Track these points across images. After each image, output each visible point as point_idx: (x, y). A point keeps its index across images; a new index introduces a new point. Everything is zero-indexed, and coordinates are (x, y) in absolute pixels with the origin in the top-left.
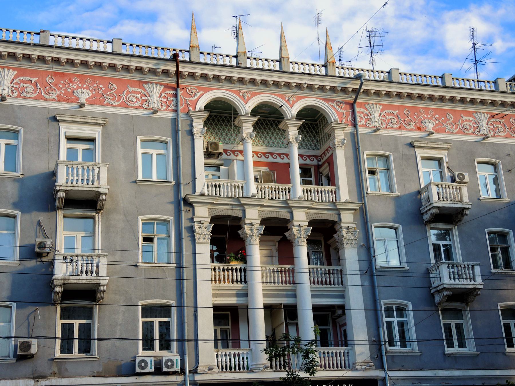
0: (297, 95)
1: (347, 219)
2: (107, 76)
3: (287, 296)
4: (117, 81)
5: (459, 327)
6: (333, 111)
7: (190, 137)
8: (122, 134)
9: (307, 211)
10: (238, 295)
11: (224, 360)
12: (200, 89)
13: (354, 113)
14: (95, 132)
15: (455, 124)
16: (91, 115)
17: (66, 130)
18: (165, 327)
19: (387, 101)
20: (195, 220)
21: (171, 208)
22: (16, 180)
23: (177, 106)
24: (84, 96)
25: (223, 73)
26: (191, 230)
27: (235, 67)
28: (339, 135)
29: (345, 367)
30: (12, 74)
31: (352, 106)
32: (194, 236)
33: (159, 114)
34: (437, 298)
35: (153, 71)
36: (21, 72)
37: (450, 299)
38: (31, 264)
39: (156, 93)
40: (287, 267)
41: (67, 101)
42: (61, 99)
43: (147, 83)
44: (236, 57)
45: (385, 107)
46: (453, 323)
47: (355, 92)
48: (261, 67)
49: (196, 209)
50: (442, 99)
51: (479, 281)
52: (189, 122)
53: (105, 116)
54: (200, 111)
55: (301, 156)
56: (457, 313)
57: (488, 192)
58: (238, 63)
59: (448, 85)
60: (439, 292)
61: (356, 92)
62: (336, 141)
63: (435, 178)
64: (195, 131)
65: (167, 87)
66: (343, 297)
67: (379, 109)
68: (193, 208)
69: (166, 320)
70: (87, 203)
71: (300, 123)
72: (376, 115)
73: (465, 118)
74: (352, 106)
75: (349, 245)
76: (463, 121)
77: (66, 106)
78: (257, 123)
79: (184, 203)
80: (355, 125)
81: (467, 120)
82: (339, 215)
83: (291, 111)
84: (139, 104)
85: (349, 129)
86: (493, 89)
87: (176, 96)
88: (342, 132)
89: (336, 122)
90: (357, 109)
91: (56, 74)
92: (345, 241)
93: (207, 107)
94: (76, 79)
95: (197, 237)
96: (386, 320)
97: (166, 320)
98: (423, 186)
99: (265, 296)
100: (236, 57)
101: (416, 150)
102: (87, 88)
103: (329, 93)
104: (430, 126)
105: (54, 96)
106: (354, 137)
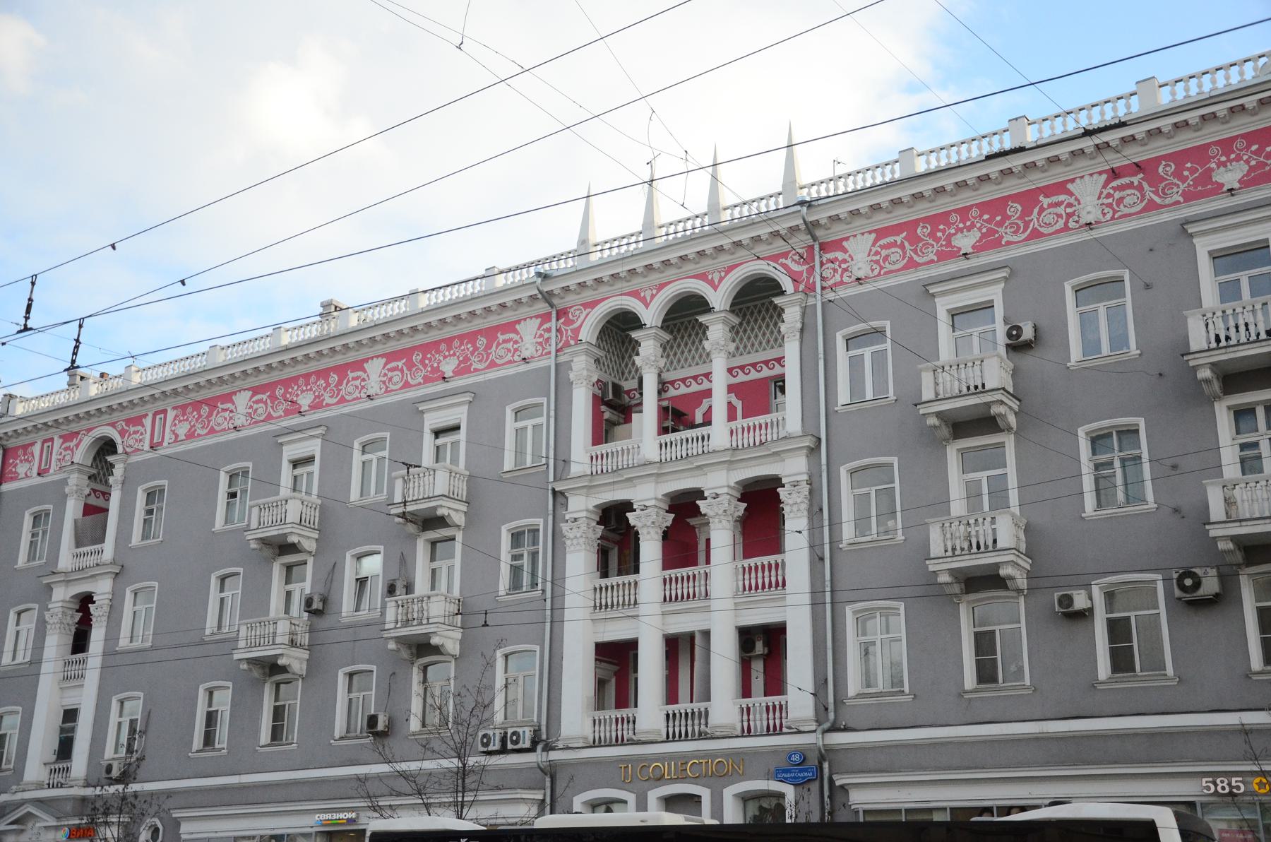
92: (568, 542)
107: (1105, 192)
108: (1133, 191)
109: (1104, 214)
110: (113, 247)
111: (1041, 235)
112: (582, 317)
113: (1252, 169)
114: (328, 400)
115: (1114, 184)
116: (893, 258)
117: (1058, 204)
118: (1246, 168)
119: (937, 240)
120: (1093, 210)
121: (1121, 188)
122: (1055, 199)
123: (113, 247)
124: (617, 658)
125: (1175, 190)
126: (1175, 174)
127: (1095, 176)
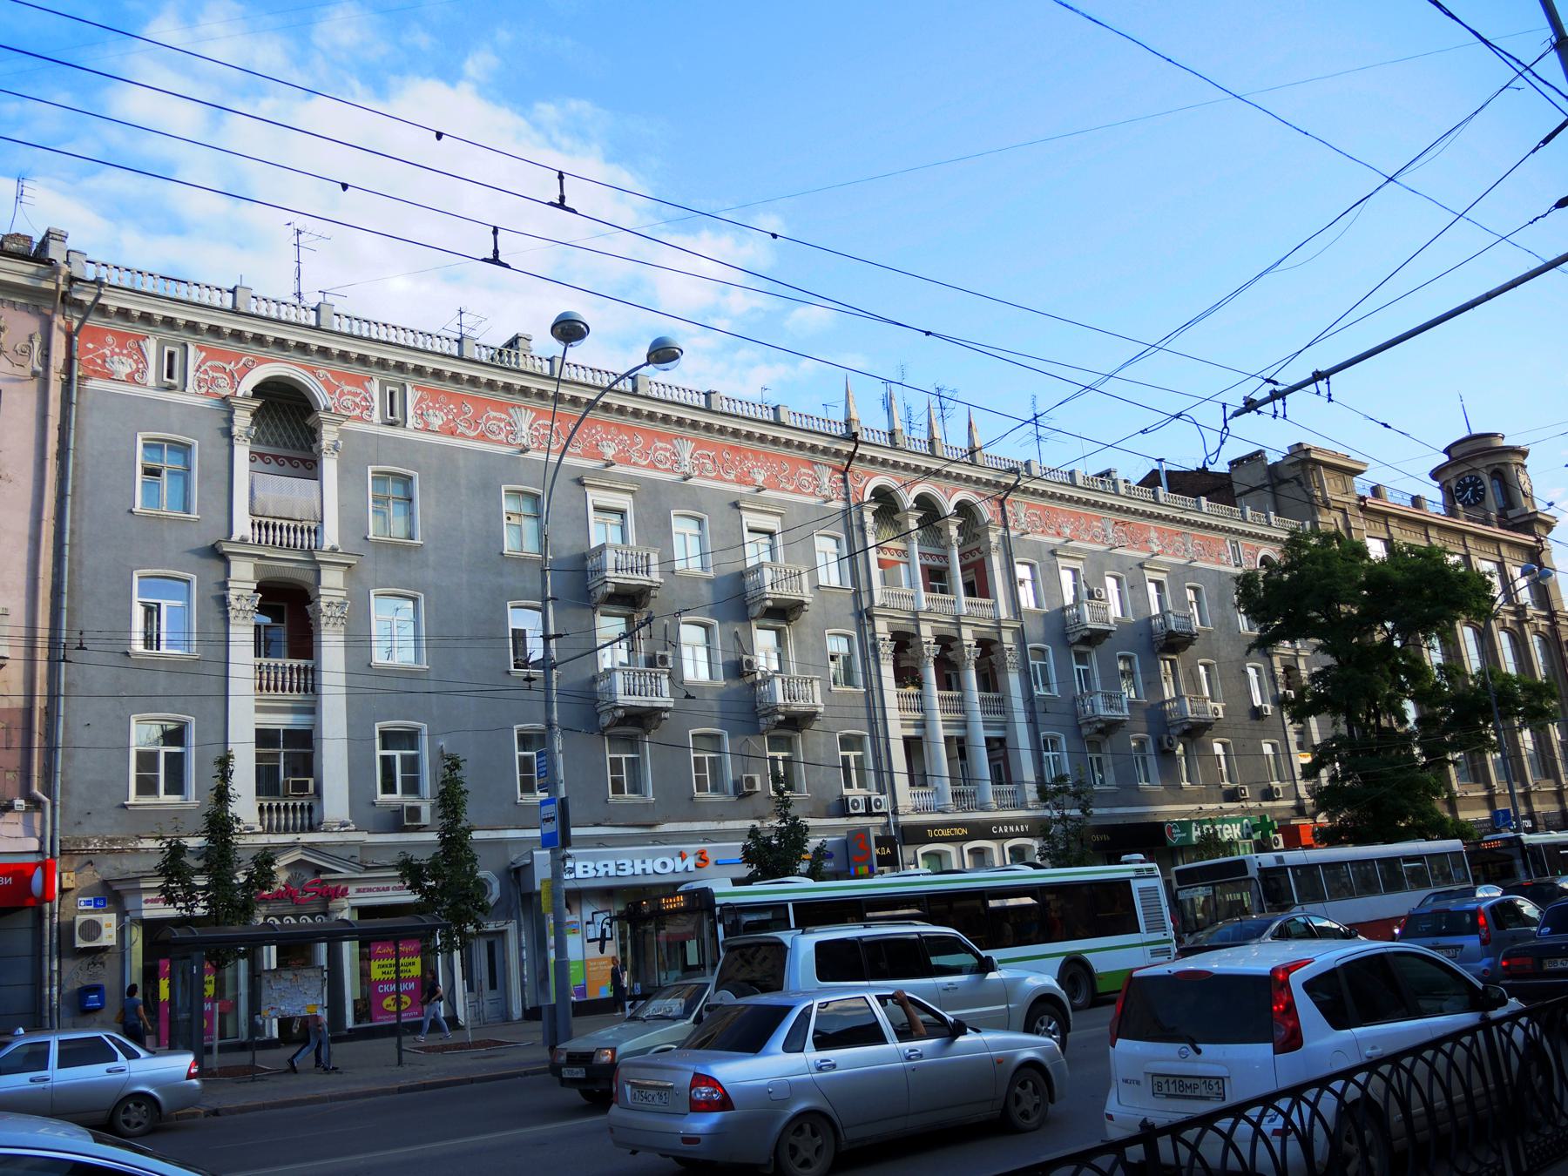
0: (254, 353)
1: (1007, 638)
2: (480, 396)
3: (958, 727)
4: (790, 460)
5: (1098, 760)
6: (987, 511)
7: (226, 440)
8: (799, 530)
9: (256, 560)
10: (915, 726)
11: (922, 801)
12: (867, 474)
13: (1003, 510)
14: (625, 501)
15: (474, 422)
16: (767, 502)
17: (595, 497)
18: (412, 764)
19: (703, 436)
20: (230, 584)
21: (852, 620)
22: (709, 581)
23: (847, 494)
24: (610, 452)
25: (293, 337)
26: (875, 647)
27: (310, 327)
28: (994, 538)
29: (1015, 806)
30: (690, 446)
31: (1001, 502)
32: (227, 612)
33: (531, 455)
34: (1086, 731)
35: (825, 451)
36: (700, 444)
37: (621, 722)
38: (736, 684)
39: (827, 478)
40: (302, 663)
41: (746, 483)
42: (740, 481)
43: (513, 406)
44: (233, 292)
45: (1030, 506)
46: (1094, 756)
47: (1011, 484)
48: (264, 314)
49: (233, 565)
50: (456, 377)
51: (1127, 712)
52: (225, 415)
53: (781, 503)
54: (245, 397)
55: (922, 554)
56: (632, 743)
57: (1115, 611)
58: (635, 389)
59: (466, 355)
60: (765, 716)
61: (851, 457)
62: (324, 444)
63: (614, 537)
64: (235, 430)
65: (836, 469)
66: (1004, 728)
67: (690, 446)
68: (228, 563)
69: (177, 749)
70: (783, 613)
71: (257, 404)
72: (525, 427)
73: (659, 444)
74: (1001, 502)
75: (239, 621)
76: (488, 419)
77: (745, 489)
78: (259, 409)
79: (864, 616)
80: (1006, 527)
81: (349, 393)
82: (318, 572)
83: (908, 499)
84: (357, 412)
85: (1001, 531)
86: (703, 404)
87: (845, 481)
88: (334, 428)
89: (327, 410)
90: (1008, 508)
91: (731, 448)
92: (323, 620)
93: (259, 391)
94: (109, 339)
95: (232, 614)
96: (841, 753)
97: (177, 749)
98: (593, 545)
99: (945, 727)
100: (233, 292)
101: (744, 513)
102: (440, 409)
103: (315, 357)
104: (610, 452)
105: (732, 477)
106: (1006, 541)
111: (656, 467)
117: (501, 420)
121: (215, 369)
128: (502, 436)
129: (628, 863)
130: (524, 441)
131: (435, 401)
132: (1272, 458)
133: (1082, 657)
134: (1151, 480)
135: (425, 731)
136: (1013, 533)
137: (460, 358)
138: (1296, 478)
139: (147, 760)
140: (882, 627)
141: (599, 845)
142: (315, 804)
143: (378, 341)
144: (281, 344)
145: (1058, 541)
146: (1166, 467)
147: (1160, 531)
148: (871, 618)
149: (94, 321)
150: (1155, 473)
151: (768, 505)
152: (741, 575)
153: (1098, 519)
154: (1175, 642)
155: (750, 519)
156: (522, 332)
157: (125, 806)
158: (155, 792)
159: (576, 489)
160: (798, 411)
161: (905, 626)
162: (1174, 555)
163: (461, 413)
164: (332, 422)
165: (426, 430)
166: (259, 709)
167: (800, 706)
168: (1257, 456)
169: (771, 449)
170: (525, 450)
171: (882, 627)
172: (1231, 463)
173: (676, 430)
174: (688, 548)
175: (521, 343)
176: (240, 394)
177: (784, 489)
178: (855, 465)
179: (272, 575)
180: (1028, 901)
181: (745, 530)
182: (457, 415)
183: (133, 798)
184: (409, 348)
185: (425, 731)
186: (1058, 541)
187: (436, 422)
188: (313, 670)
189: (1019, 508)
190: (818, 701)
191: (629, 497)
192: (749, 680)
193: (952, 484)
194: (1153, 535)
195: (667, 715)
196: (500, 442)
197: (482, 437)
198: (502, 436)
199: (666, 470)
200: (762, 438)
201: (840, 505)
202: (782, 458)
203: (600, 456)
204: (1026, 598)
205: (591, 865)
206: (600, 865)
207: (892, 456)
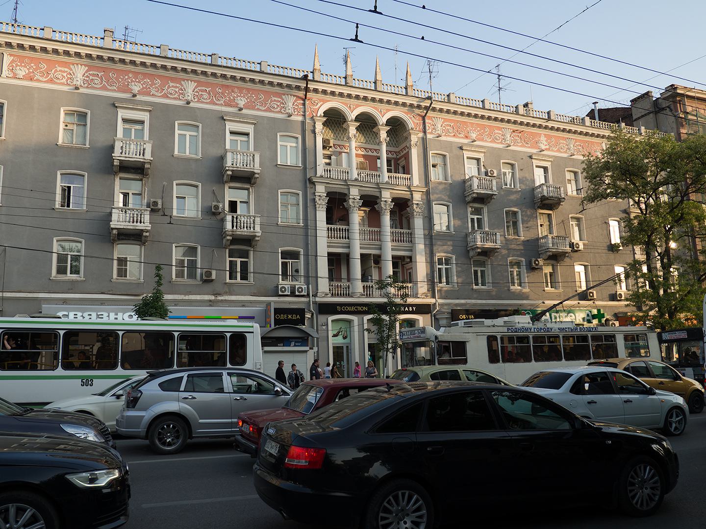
4: (264, 92)
5: (483, 272)
6: (412, 121)
12: (321, 100)
13: (424, 123)
16: (246, 116)
19: (202, 78)
20: (316, 194)
21: (300, 185)
23: (305, 112)
28: (414, 139)
30: (194, 85)
31: (424, 118)
32: (315, 205)
34: (471, 254)
36: (199, 83)
41: (231, 106)
42: (227, 104)
45: (446, 120)
54: (320, 116)
64: (317, 131)
66: (411, 250)
67: (83, 69)
75: (320, 209)
78: (325, 121)
80: (425, 132)
85: (421, 135)
87: (304, 104)
90: (427, 121)
91: (223, 86)
92: (415, 214)
93: (326, 113)
94: (236, 90)
95: (317, 206)
104: (474, 136)
105: (222, 102)
106: (424, 140)
107: (86, 75)
108: (98, 79)
109: (194, 99)
110: (423, 38)
111: (167, 97)
112: (319, 105)
113: (143, 88)
114: (153, 92)
115: (91, 72)
116: (96, 82)
117: (64, 72)
118: (27, 72)
119: (119, 82)
120: (80, 81)
121: (93, 75)
122: (63, 69)
123: (423, 38)
124: (338, 262)
125: (115, 85)
126: (116, 79)
127: (83, 66)
128: (64, 81)
129: (105, 314)
130: (439, 132)
131: (22, 62)
132: (656, 94)
133: (477, 211)
134: (591, 114)
135: (302, 253)
136: (429, 136)
137: (376, 90)
138: (668, 107)
139: (181, 263)
140: (321, 189)
141: (102, 304)
142: (350, 285)
143: (536, 118)
144: (333, 93)
145: (466, 141)
146: (599, 106)
147: (548, 137)
148: (313, 183)
149: (430, 114)
150: (593, 111)
151: (243, 118)
152: (464, 181)
153: (499, 128)
154: (550, 203)
155: (535, 163)
156: (529, 101)
157: (50, 279)
158: (66, 273)
159: (113, 109)
160: (559, 114)
161: (338, 188)
162: (558, 151)
163: (38, 68)
164: (414, 135)
165: (15, 77)
166: (328, 246)
167: (244, 232)
168: (647, 94)
169: (250, 85)
170: (290, 116)
171: (321, 189)
172: (632, 101)
173: (182, 75)
174: (186, 144)
175: (530, 106)
176: (318, 115)
177: (258, 109)
178: (430, 114)
179: (365, 193)
180: (170, 356)
181: (534, 167)
182: (36, 70)
183: (228, 280)
184: (477, 107)
185: (302, 253)
186: (466, 141)
187: (21, 73)
188: (411, 234)
189: (437, 124)
190: (258, 228)
191: (148, 114)
192: (219, 217)
193: (353, 101)
194: (543, 138)
195: (147, 234)
196: (63, 84)
197: (51, 81)
198: (64, 81)
199: (175, 99)
200: (476, 116)
201: (300, 118)
202: (484, 127)
203: (130, 91)
204: (436, 175)
205: (79, 314)
206: (87, 317)
207: (346, 91)
